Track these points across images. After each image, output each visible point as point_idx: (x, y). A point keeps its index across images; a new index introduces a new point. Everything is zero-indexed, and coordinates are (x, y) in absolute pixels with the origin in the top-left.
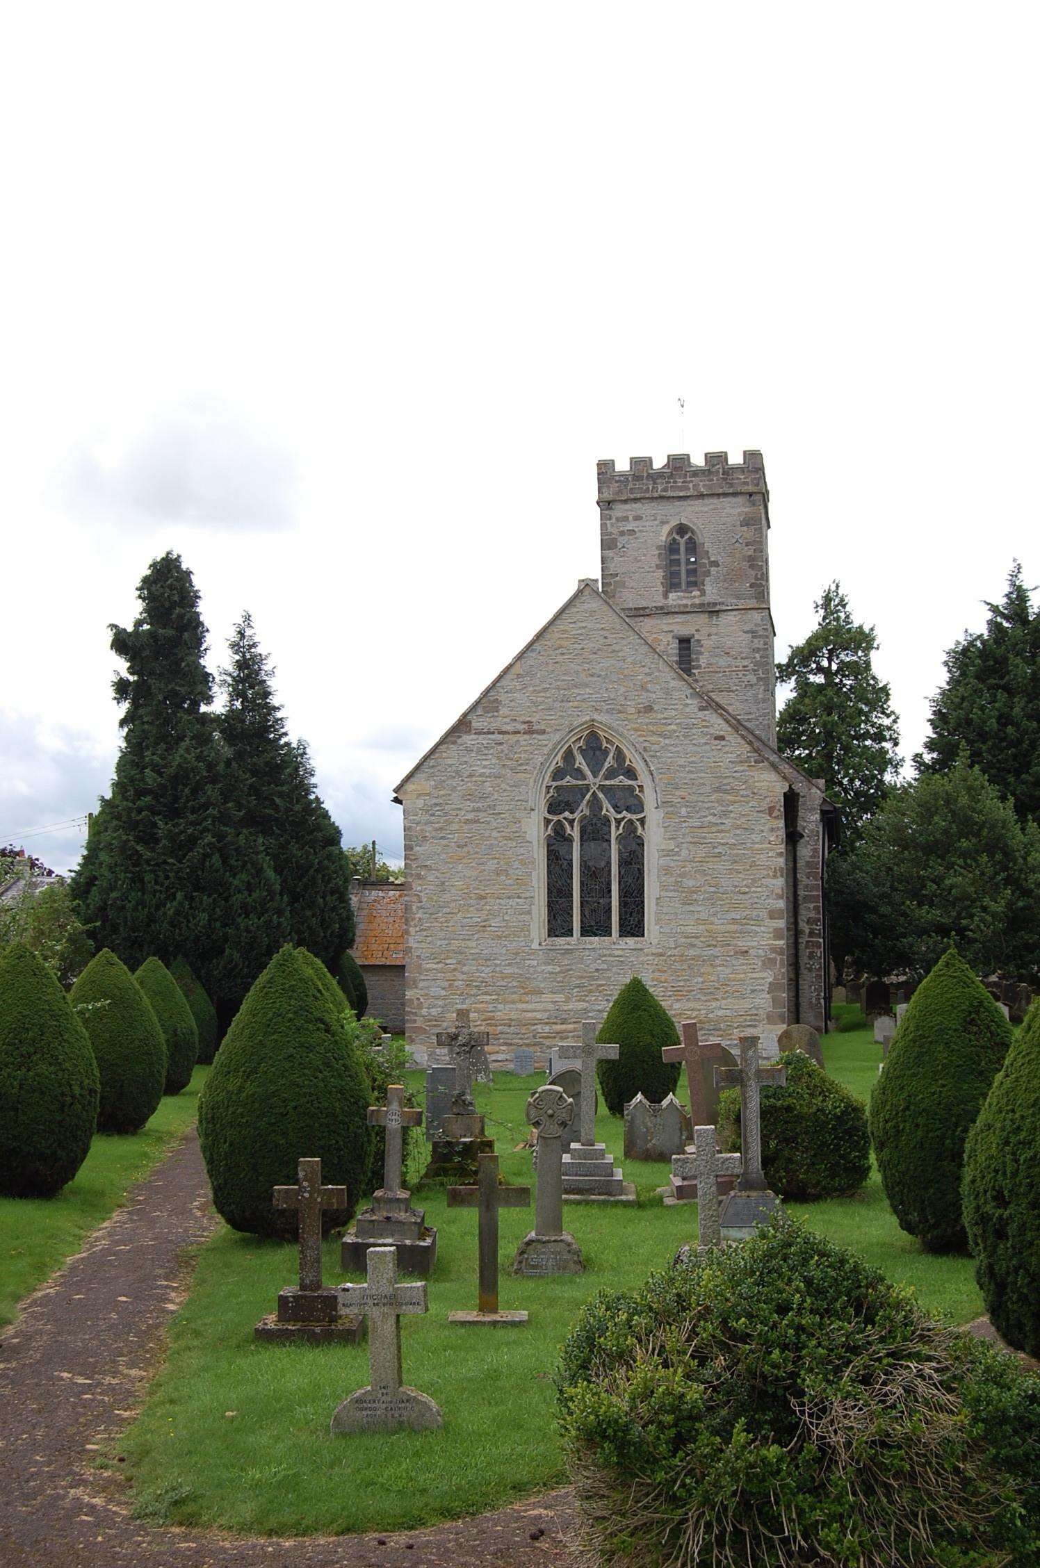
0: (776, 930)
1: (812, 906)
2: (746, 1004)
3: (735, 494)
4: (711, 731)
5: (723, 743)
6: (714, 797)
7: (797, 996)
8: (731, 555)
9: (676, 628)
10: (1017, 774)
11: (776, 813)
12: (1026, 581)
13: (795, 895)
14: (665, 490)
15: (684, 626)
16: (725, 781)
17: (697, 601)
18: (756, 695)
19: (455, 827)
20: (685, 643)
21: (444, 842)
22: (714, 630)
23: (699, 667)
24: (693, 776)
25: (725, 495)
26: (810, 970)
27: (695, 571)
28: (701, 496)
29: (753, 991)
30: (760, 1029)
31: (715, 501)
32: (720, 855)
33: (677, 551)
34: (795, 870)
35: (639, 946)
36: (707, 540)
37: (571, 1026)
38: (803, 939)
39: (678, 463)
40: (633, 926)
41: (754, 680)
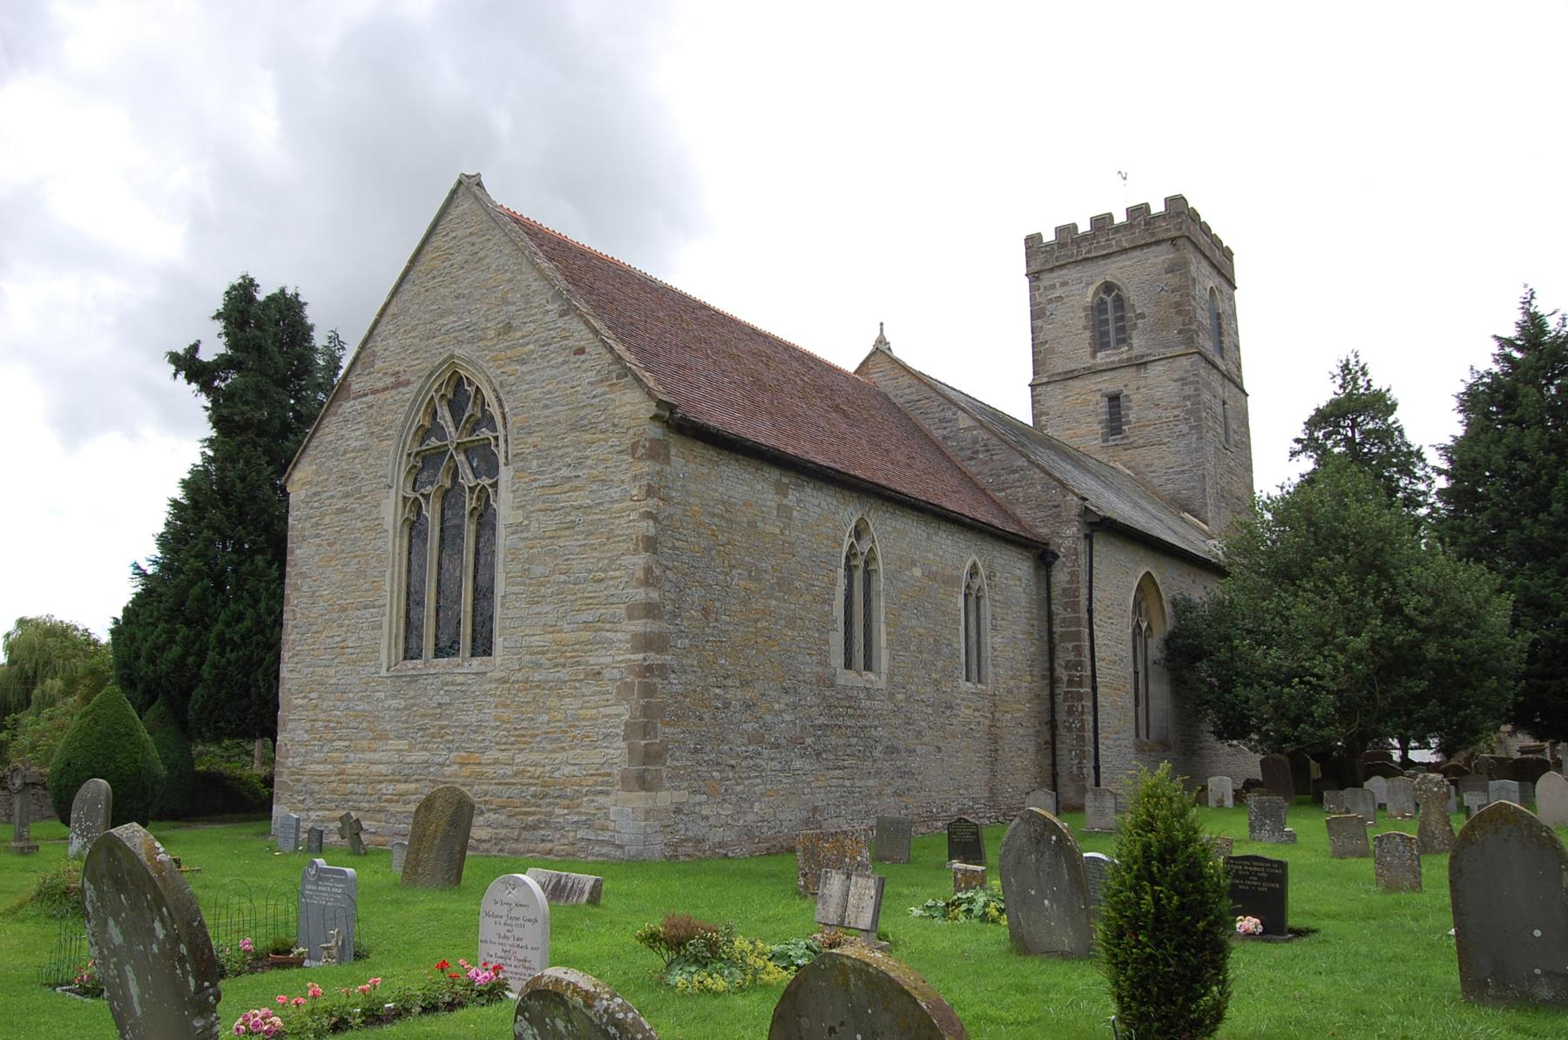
0: (635, 636)
1: (1070, 646)
2: (595, 757)
3: (1158, 243)
4: (570, 343)
5: (583, 357)
6: (569, 438)
7: (1054, 765)
8: (1157, 304)
9: (1104, 386)
10: (1534, 514)
11: (640, 451)
12: (1541, 306)
13: (1050, 632)
14: (1089, 252)
15: (1109, 383)
16: (583, 413)
17: (1125, 356)
18: (1188, 445)
19: (327, 520)
20: (1114, 399)
21: (318, 541)
22: (1142, 383)
23: (1129, 422)
24: (547, 412)
25: (1148, 245)
26: (1070, 730)
27: (1123, 328)
28: (1124, 251)
29: (606, 736)
30: (612, 798)
31: (1138, 253)
32: (572, 526)
33: (1105, 311)
34: (1049, 599)
35: (483, 668)
36: (1132, 295)
37: (413, 786)
38: (1062, 689)
39: (1102, 223)
40: (483, 645)
41: (1184, 428)
